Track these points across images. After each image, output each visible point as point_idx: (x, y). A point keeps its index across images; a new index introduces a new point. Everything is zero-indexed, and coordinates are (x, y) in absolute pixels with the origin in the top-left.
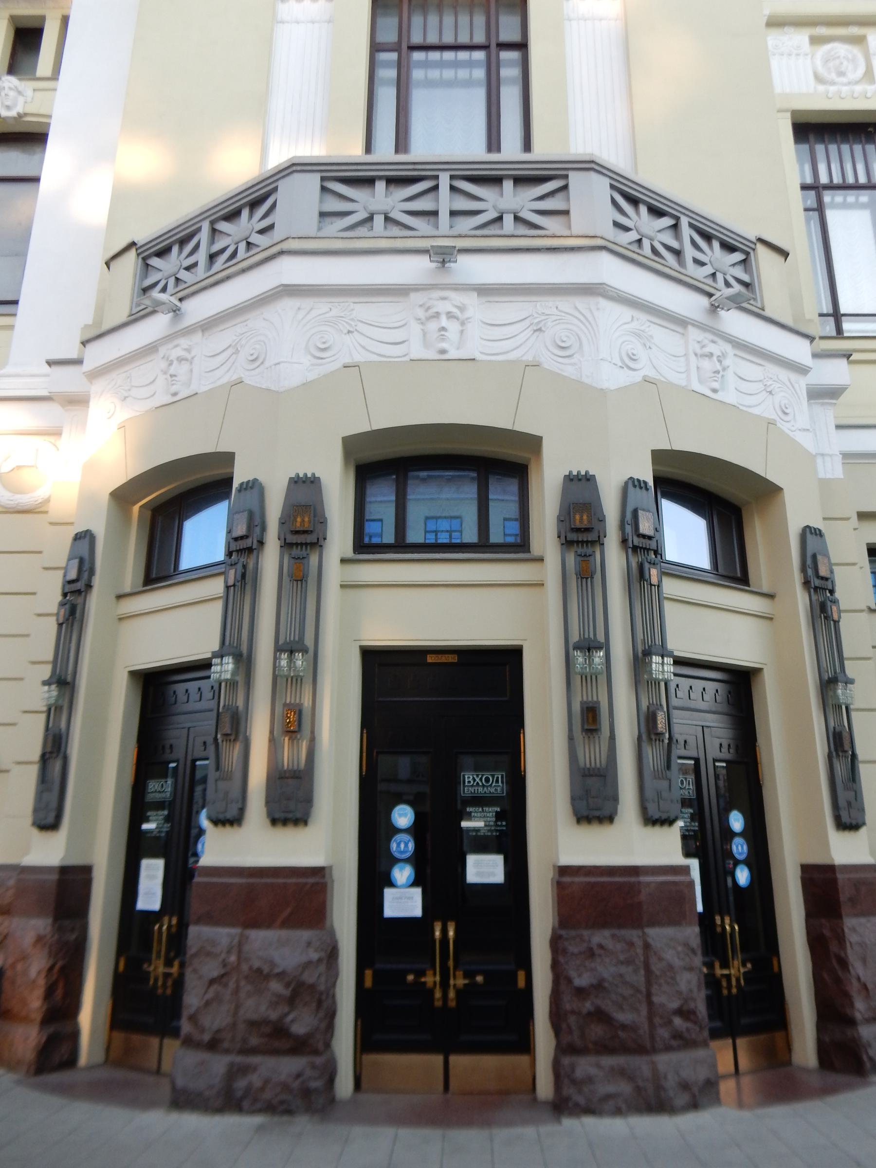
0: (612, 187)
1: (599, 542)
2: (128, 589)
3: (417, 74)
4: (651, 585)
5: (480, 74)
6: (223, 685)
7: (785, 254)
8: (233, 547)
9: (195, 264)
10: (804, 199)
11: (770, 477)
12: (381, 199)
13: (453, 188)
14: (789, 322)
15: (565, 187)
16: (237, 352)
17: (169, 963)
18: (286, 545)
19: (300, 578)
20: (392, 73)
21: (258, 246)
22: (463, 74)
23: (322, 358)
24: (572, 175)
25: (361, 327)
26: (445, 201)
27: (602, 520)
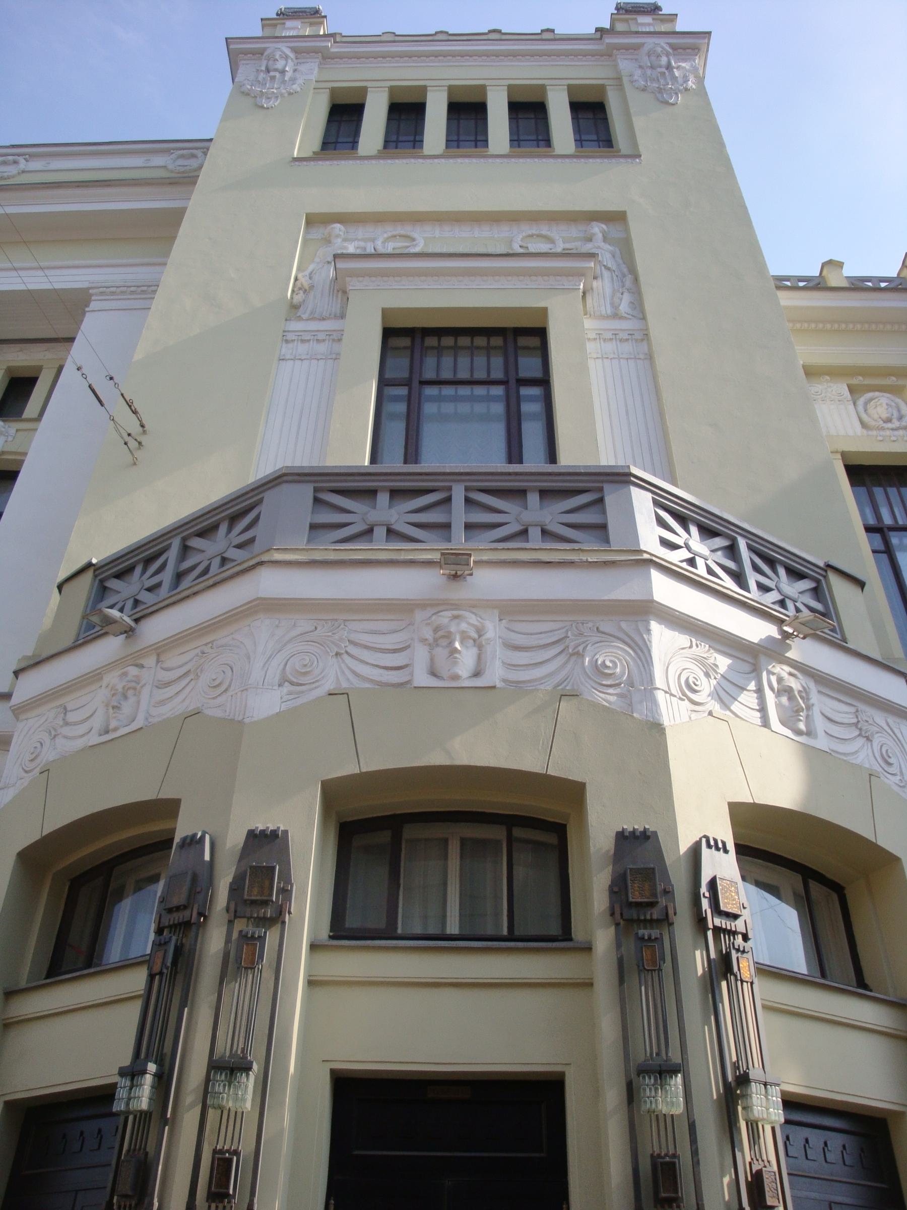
0: (656, 503)
1: (666, 920)
2: (23, 984)
3: (429, 409)
4: (742, 981)
5: (499, 408)
6: (131, 1118)
7: (861, 584)
8: (165, 922)
9: (159, 585)
10: (871, 542)
11: (882, 842)
12: (386, 512)
13: (468, 501)
14: (878, 657)
15: (601, 501)
16: (198, 676)
17: (780, 680)
18: (234, 914)
19: (243, 958)
20: (402, 408)
21: (234, 561)
22: (480, 408)
23: (301, 685)
24: (607, 488)
25: (352, 650)
26: (459, 514)
27: (668, 893)
